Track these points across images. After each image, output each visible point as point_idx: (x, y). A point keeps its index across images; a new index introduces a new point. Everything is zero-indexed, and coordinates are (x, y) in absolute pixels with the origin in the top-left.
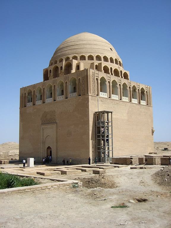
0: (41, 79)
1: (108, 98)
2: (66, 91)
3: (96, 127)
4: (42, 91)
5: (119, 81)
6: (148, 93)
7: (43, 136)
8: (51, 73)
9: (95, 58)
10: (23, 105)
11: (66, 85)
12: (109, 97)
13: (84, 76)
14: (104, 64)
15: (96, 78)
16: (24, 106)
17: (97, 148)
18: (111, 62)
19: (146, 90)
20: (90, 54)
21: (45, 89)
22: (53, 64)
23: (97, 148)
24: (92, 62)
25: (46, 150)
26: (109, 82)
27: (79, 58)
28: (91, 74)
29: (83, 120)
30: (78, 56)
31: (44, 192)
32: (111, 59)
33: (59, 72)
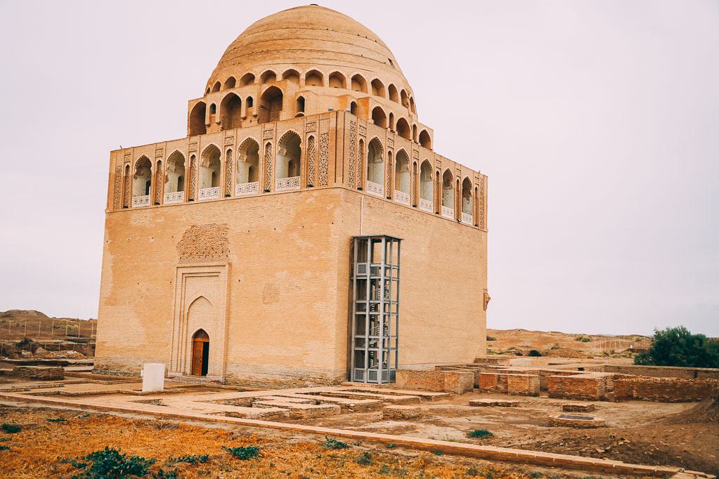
5: (413, 154)
7: (183, 298)
8: (215, 113)
10: (119, 201)
11: (192, 163)
12: (388, 198)
13: (326, 131)
16: (120, 205)
17: (353, 340)
21: (130, 168)
22: (221, 88)
23: (353, 340)
24: (341, 92)
25: (190, 340)
26: (390, 153)
27: (303, 77)
29: (315, 258)
32: (392, 88)
33: (243, 114)
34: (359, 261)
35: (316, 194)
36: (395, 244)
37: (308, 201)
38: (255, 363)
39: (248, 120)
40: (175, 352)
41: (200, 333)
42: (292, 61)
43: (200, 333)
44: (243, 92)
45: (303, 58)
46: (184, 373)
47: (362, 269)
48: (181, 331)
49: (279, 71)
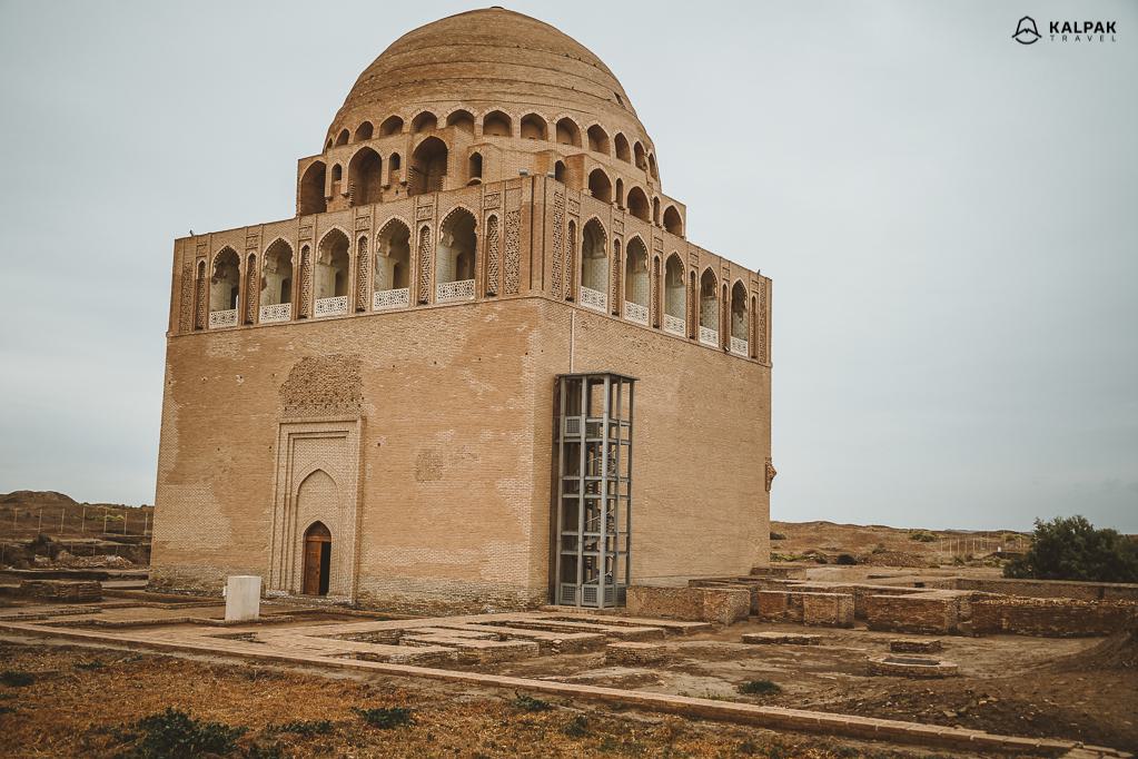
0: (289, 209)
1: (610, 316)
2: (421, 272)
3: (561, 446)
4: (240, 267)
6: (758, 302)
7: (290, 470)
8: (340, 179)
9: (552, 129)
13: (516, 208)
14: (594, 161)
15: (569, 218)
16: (190, 324)
17: (559, 538)
18: (618, 157)
19: (753, 295)
20: (530, 112)
22: (351, 140)
23: (559, 538)
24: (541, 145)
25: (301, 539)
26: (617, 242)
27: (480, 121)
28: (551, 200)
29: (499, 409)
30: (475, 114)
31: (692, 686)
32: (620, 140)
33: (385, 181)
34: (568, 413)
35: (499, 307)
36: (626, 387)
37: (488, 318)
38: (403, 575)
39: (393, 190)
40: (277, 558)
41: (317, 528)
42: (462, 97)
43: (317, 528)
44: (385, 147)
45: (479, 92)
46: (292, 592)
47: (574, 427)
48: (286, 526)
49: (442, 112)
